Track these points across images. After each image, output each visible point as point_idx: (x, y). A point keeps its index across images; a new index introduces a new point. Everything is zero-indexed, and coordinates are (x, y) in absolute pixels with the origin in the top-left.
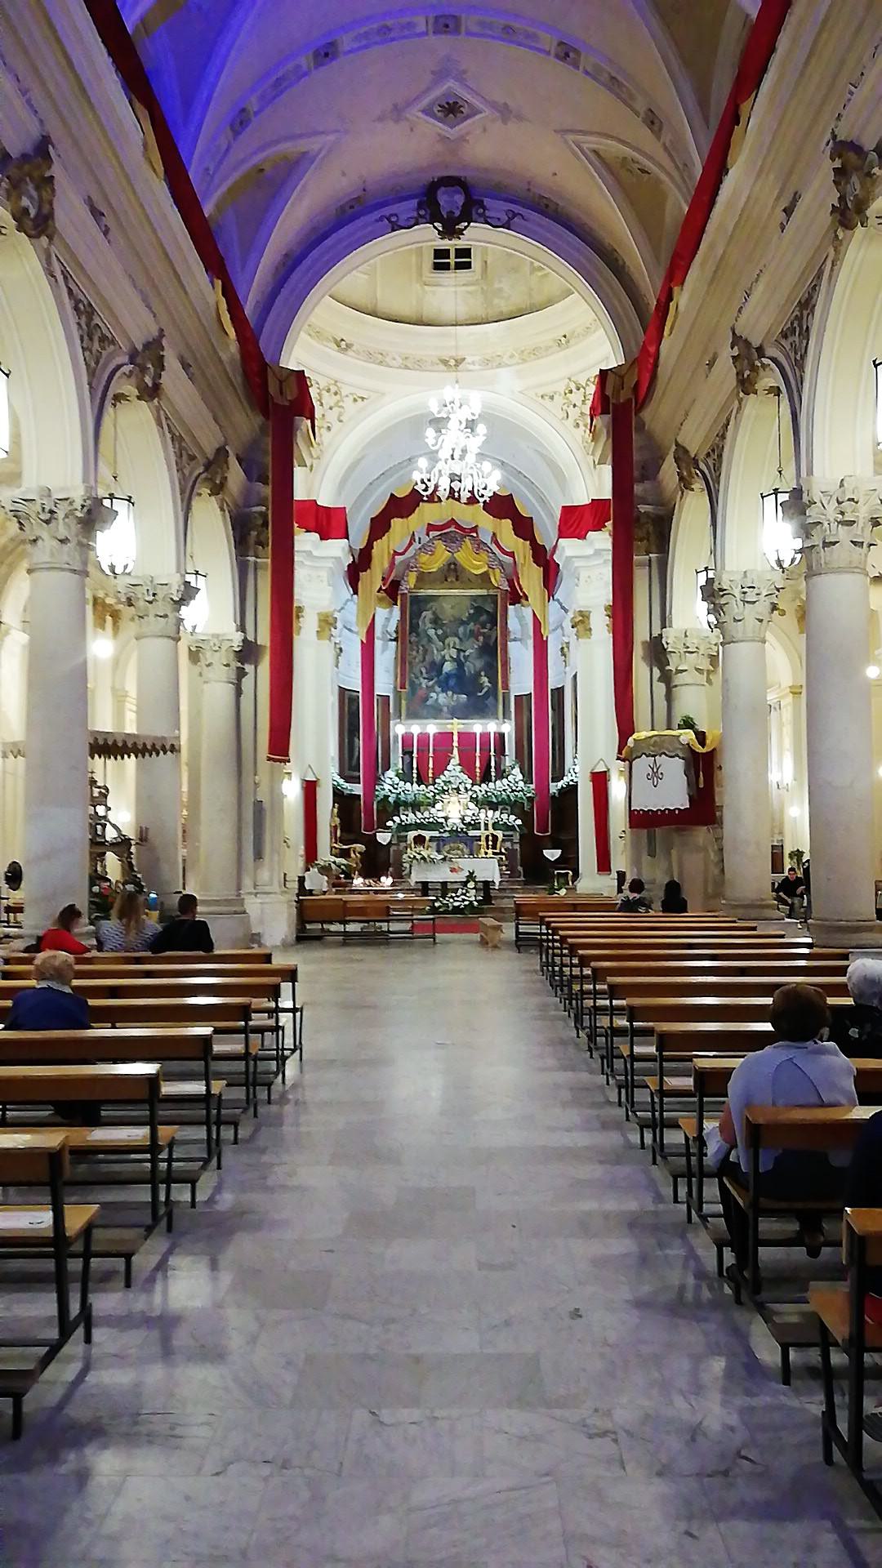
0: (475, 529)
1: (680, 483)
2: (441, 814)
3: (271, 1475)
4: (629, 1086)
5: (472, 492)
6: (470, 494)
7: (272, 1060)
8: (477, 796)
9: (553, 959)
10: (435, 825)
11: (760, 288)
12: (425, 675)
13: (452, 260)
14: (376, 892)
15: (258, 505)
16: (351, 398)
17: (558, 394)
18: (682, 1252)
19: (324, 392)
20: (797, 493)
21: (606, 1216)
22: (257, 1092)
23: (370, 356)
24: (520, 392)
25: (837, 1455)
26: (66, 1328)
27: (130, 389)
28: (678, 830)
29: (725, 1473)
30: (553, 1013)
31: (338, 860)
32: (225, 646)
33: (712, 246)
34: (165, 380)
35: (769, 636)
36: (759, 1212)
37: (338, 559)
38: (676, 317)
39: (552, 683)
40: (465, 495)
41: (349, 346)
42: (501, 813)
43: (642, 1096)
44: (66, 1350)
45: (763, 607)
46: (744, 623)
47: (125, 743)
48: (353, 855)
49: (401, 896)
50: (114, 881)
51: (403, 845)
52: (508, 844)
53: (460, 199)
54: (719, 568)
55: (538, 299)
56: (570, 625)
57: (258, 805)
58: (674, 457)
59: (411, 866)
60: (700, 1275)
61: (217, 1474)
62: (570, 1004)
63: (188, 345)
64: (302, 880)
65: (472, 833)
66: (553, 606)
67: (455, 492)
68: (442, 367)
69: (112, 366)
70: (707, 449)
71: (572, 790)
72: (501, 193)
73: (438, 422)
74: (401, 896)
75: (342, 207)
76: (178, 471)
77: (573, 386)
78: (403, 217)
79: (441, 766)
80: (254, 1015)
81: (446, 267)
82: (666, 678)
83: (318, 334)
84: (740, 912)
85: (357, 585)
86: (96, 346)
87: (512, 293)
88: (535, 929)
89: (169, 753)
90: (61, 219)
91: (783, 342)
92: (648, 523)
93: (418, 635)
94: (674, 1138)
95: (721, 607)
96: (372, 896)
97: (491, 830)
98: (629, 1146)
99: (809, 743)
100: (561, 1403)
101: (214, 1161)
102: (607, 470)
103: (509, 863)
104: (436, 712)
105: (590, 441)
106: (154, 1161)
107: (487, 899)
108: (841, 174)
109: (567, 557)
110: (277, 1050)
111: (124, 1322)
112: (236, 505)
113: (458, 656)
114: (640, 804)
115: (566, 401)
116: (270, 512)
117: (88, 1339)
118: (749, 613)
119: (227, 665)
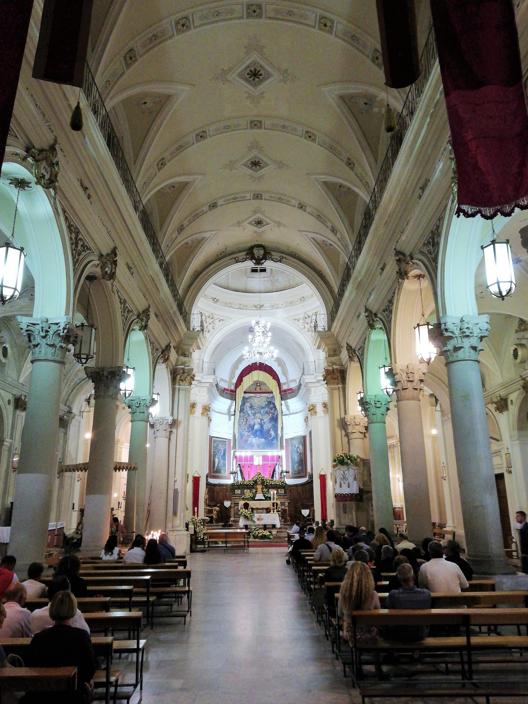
15: (181, 365)
23: (226, 304)
32: (165, 422)
34: (150, 323)
41: (218, 300)
53: (262, 252)
54: (365, 392)
63: (158, 309)
68: (254, 308)
69: (132, 319)
71: (310, 483)
72: (277, 250)
77: (306, 316)
78: (240, 258)
87: (282, 281)
90: (61, 182)
95: (367, 409)
103: (283, 515)
108: (399, 261)
113: (261, 421)
114: (339, 491)
118: (379, 412)
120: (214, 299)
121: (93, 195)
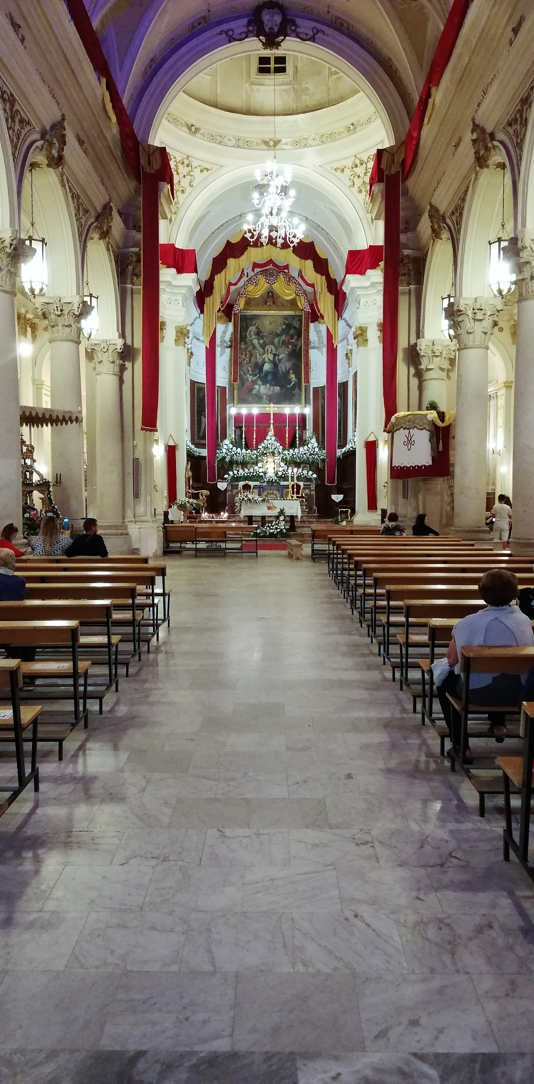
0: (287, 267)
1: (432, 234)
2: (261, 470)
3: (157, 865)
4: (386, 643)
5: (285, 239)
6: (283, 241)
7: (151, 626)
8: (286, 458)
9: (337, 566)
10: (258, 477)
11: (494, 88)
12: (251, 373)
13: (272, 65)
14: (217, 522)
15: (133, 247)
16: (199, 169)
17: (347, 168)
18: (418, 742)
19: (179, 164)
20: (514, 241)
21: (369, 720)
22: (141, 646)
24: (319, 166)
25: (512, 855)
26: (23, 782)
27: (41, 159)
28: (423, 480)
29: (442, 865)
30: (336, 600)
31: (191, 500)
33: (461, 56)
34: (66, 153)
35: (491, 345)
36: (468, 712)
37: (190, 288)
38: (433, 109)
39: (340, 378)
40: (280, 241)
41: (197, 130)
42: (303, 470)
43: (394, 650)
44: (23, 795)
45: (487, 323)
46: (474, 336)
47: (44, 414)
48: (201, 497)
49: (233, 525)
50: (39, 510)
51: (235, 491)
52: (307, 491)
53: (278, 19)
55: (333, 96)
56: (353, 337)
57: (136, 462)
58: (429, 215)
59: (240, 506)
60: (430, 755)
61: (123, 864)
62: (348, 594)
64: (166, 514)
65: (283, 483)
66: (341, 324)
67: (273, 239)
68: (264, 147)
70: (452, 208)
71: (352, 453)
72: (309, 15)
73: (261, 188)
74: (233, 525)
75: (192, 24)
76: (77, 221)
77: (358, 162)
78: (237, 32)
79: (262, 437)
80: (138, 598)
81: (267, 71)
82: (419, 374)
83: (175, 121)
84: (465, 535)
85: (203, 307)
86: (17, 127)
88: (325, 547)
89: (74, 422)
91: (509, 128)
92: (408, 263)
93: (246, 343)
94: (414, 675)
96: (214, 525)
97: (296, 481)
98: (386, 680)
99: (515, 418)
100: (338, 827)
101: (114, 687)
102: (381, 224)
103: (307, 503)
104: (258, 399)
105: (369, 202)
106: (75, 685)
107: (293, 527)
109: (352, 287)
110: (153, 620)
111: (58, 780)
112: (119, 248)
113: (274, 358)
115: (352, 173)
116: (142, 252)
117: (37, 789)
118: (478, 328)
119: (113, 362)
120: (190, 127)
121: (27, 35)
